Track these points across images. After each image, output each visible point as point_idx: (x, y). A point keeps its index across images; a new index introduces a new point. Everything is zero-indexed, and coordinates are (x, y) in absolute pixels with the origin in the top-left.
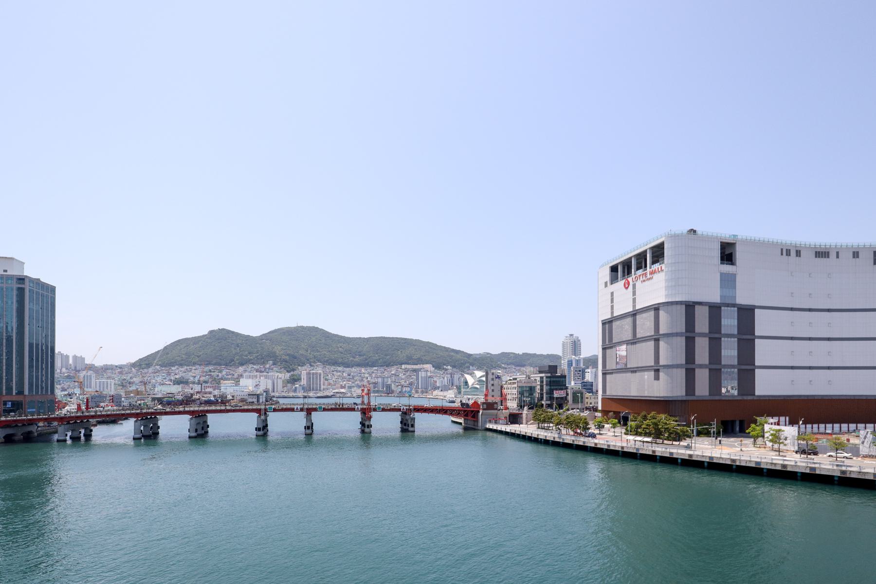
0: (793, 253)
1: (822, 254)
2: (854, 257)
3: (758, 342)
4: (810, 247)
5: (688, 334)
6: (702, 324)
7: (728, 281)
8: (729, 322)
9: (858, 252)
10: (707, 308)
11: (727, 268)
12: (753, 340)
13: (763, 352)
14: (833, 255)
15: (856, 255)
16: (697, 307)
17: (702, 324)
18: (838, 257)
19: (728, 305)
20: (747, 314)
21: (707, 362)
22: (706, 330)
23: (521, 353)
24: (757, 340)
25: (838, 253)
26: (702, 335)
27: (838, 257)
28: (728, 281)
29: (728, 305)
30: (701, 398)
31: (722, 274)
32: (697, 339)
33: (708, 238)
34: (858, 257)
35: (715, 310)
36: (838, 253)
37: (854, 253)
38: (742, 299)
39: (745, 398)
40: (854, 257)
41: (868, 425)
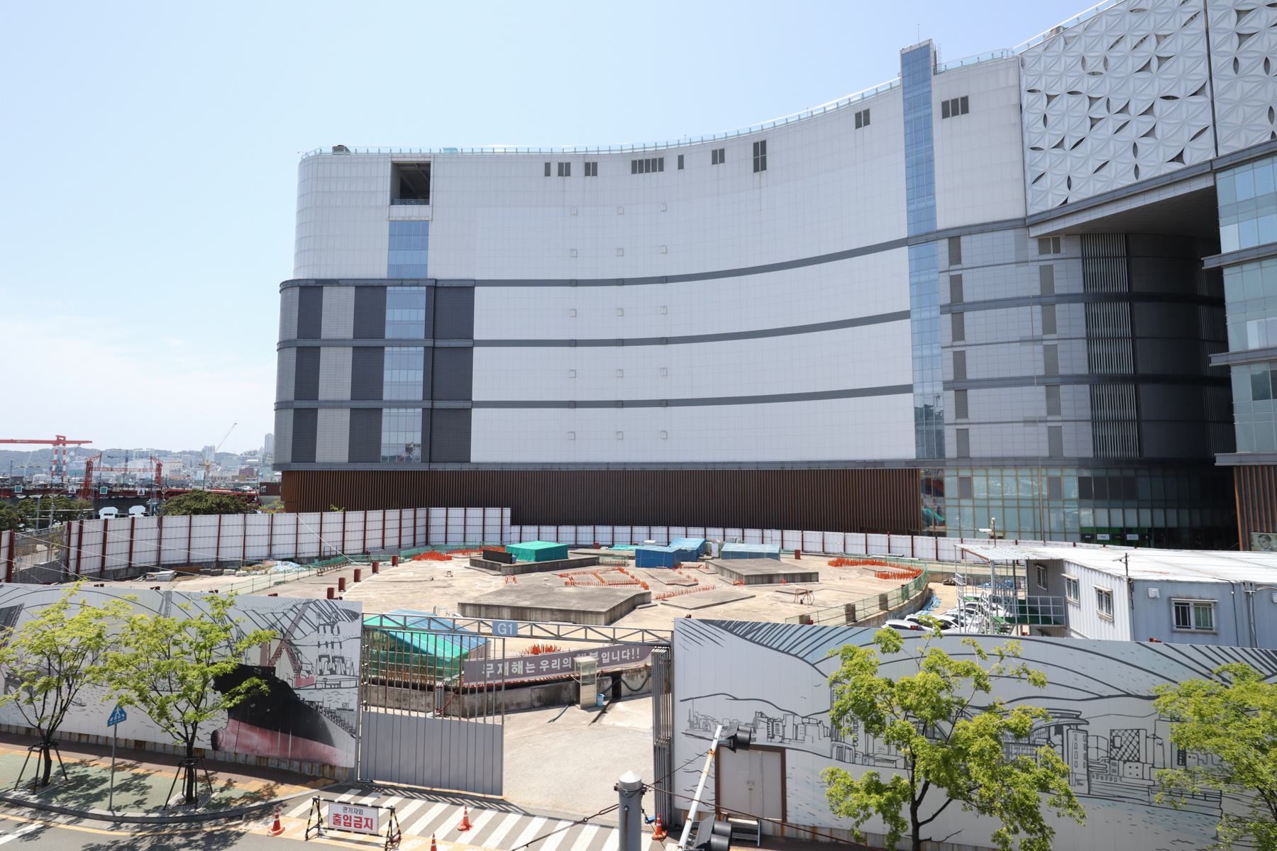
0: (577, 169)
1: (646, 164)
2: (587, 174)
3: (480, 355)
4: (622, 155)
5: (303, 343)
6: (338, 316)
7: (410, 238)
8: (406, 316)
9: (595, 164)
10: (351, 291)
11: (411, 211)
12: (468, 351)
13: (490, 374)
14: (671, 164)
15: (718, 156)
16: (327, 291)
17: (338, 316)
18: (681, 166)
19: (401, 283)
20: (450, 305)
21: (346, 394)
22: (347, 332)
23: (467, 150)
24: (477, 351)
25: (681, 159)
26: (338, 343)
27: (681, 166)
28: (410, 238)
29: (401, 283)
30: (326, 468)
31: (393, 223)
32: (324, 352)
33: (368, 159)
34: (568, 174)
35: (370, 296)
36: (681, 159)
37: (714, 153)
38: (444, 266)
39: (434, 467)
40: (587, 174)
41: (768, 532)
